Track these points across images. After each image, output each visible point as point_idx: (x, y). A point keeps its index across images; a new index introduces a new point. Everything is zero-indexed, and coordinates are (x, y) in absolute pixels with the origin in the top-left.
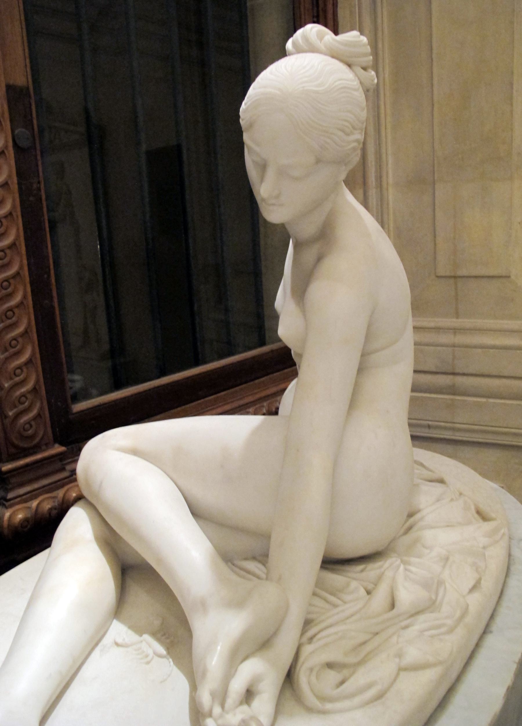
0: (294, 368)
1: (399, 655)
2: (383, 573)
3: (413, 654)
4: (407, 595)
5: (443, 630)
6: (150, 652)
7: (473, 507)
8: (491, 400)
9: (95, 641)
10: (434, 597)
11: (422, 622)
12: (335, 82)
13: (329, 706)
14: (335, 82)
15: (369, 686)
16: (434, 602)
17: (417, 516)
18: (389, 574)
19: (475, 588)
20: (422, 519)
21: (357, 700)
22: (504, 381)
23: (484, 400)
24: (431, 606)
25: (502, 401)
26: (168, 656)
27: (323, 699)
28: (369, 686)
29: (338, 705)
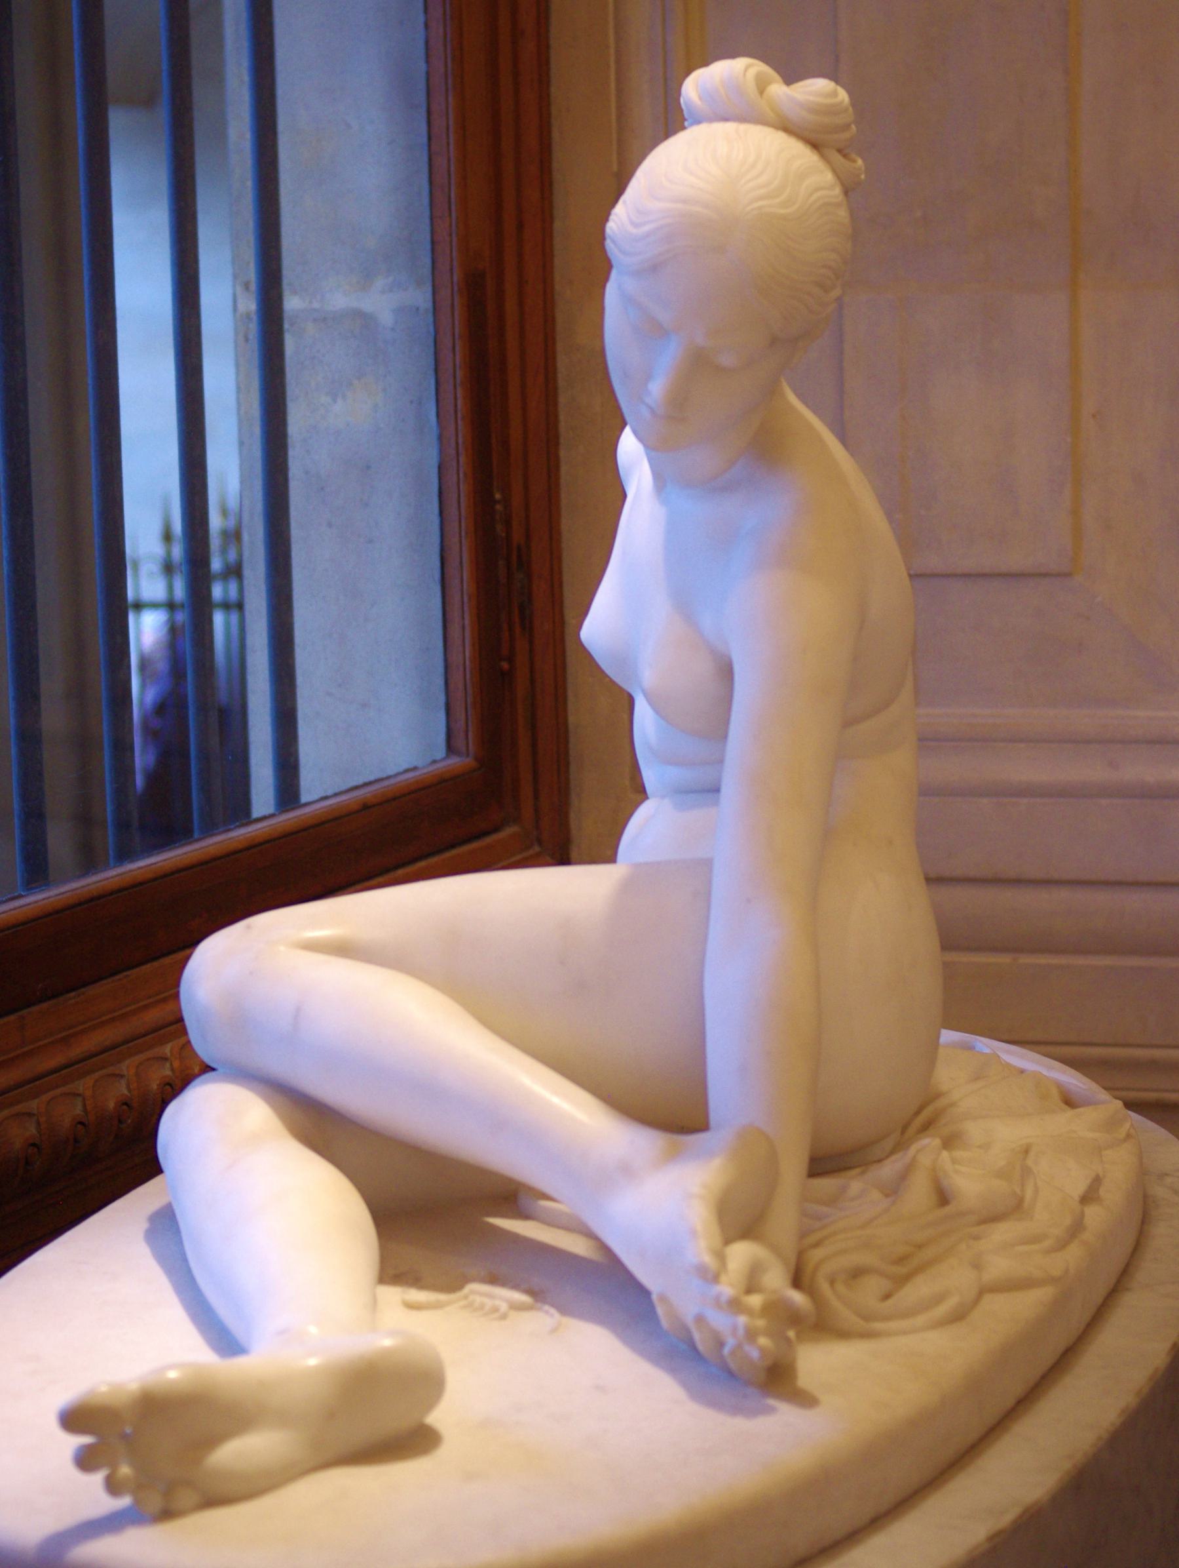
0: (183, 1040)
1: (977, 1266)
2: (914, 1159)
3: (999, 1266)
4: (970, 1182)
5: (1047, 1243)
6: (504, 1307)
7: (1055, 1092)
8: (1025, 959)
9: (374, 1303)
10: (1018, 1191)
11: (1002, 1232)
12: (811, 195)
13: (878, 1326)
14: (811, 195)
15: (939, 1299)
16: (1021, 1201)
17: (941, 1103)
18: (925, 1160)
19: (1088, 1198)
20: (953, 1105)
21: (920, 1320)
22: (1062, 895)
23: (1004, 959)
24: (1016, 1208)
25: (1062, 960)
26: (539, 1305)
27: (867, 1318)
28: (939, 1299)
29: (893, 1325)
